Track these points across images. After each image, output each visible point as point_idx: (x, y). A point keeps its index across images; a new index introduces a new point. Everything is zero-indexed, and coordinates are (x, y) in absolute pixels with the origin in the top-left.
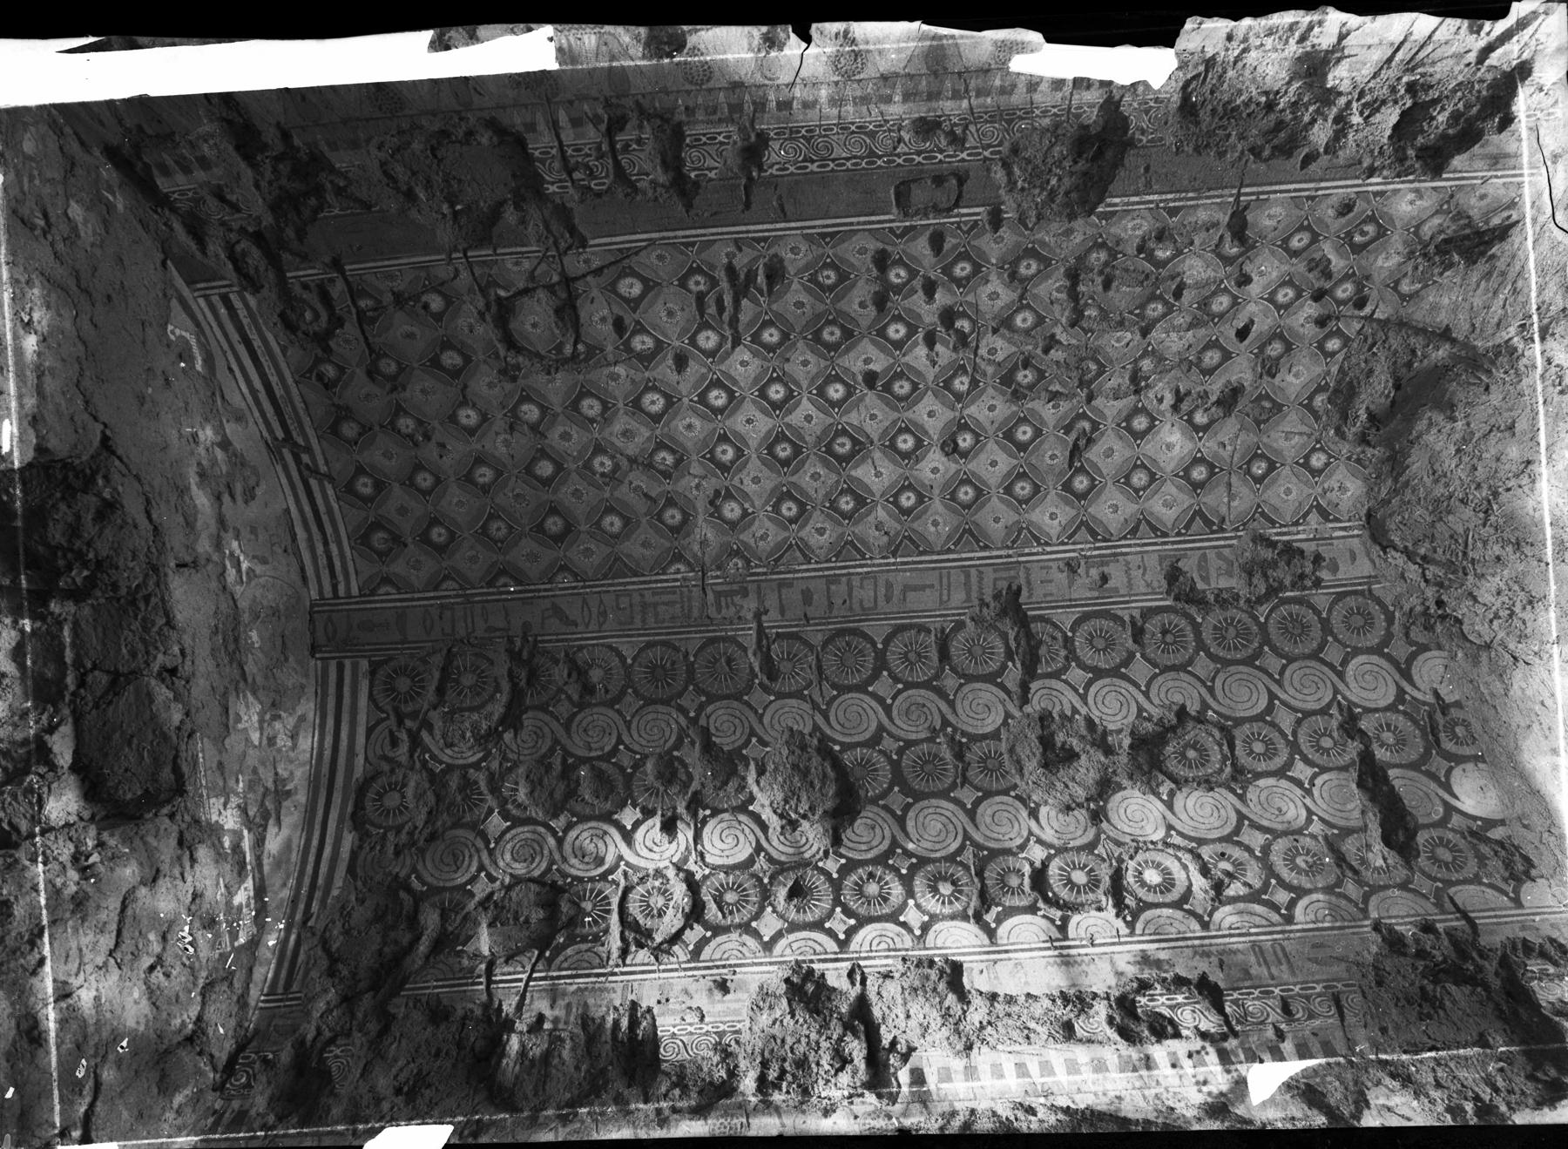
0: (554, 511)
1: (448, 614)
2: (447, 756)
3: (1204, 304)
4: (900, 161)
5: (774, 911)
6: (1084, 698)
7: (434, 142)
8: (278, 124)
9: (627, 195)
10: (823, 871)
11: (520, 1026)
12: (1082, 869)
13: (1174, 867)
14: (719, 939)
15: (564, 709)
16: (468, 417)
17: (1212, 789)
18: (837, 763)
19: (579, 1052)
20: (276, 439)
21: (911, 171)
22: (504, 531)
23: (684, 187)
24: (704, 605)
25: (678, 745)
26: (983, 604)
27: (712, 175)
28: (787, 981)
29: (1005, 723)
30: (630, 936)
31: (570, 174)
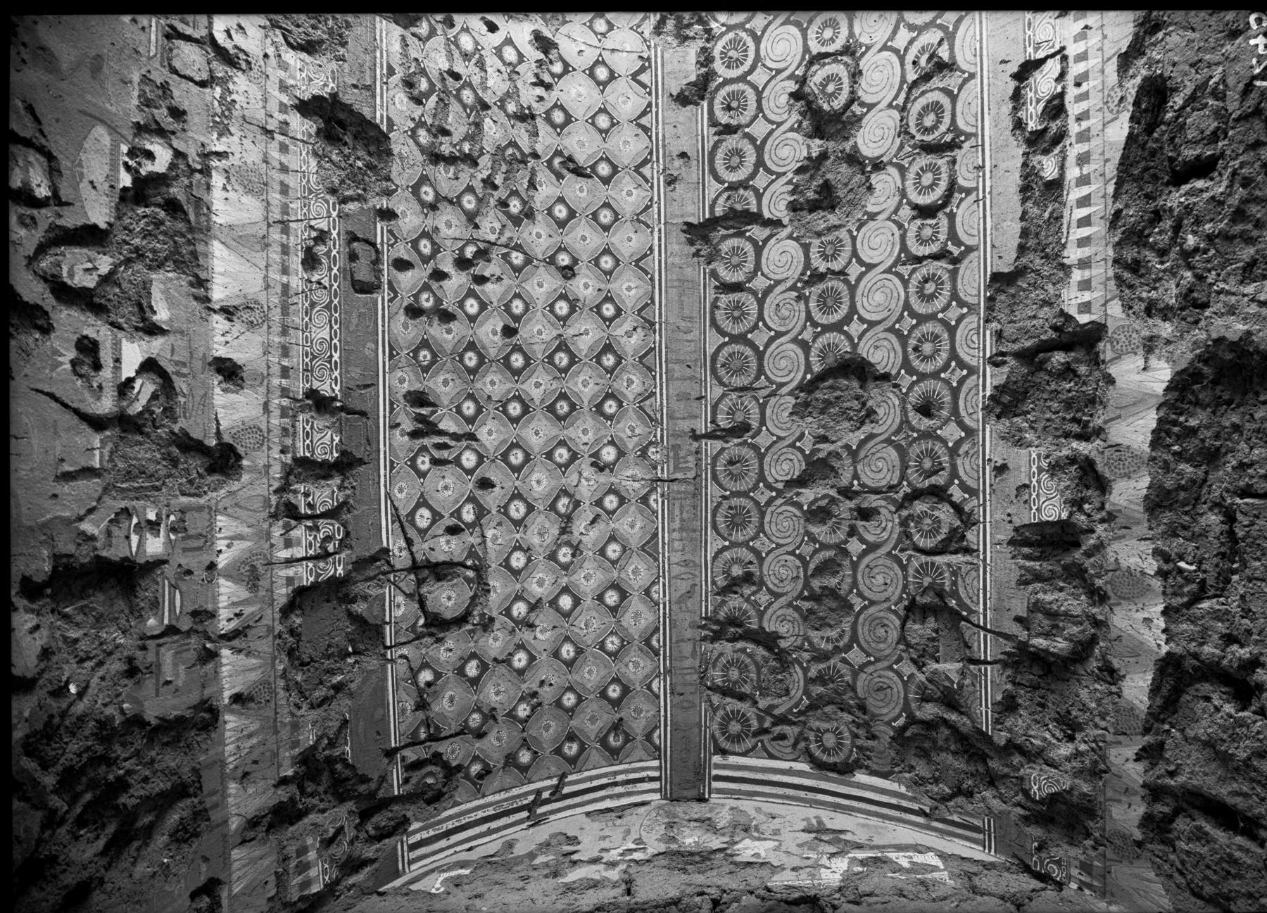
0: (600, 598)
1: (679, 689)
2: (796, 693)
3: (466, 56)
4: (336, 285)
5: (941, 428)
6: (779, 175)
7: (296, 663)
8: (274, 786)
9: (349, 511)
10: (910, 388)
11: (1023, 635)
12: (920, 177)
13: (922, 102)
14: (961, 472)
15: (763, 598)
16: (520, 660)
17: (860, 72)
18: (821, 377)
19: (1047, 588)
20: (528, 818)
21: (345, 278)
22: (614, 639)
23: (345, 465)
24: (684, 481)
25: (798, 506)
26: (697, 254)
27: (337, 439)
28: (999, 417)
29: (797, 239)
30: (954, 546)
31: (329, 555)
